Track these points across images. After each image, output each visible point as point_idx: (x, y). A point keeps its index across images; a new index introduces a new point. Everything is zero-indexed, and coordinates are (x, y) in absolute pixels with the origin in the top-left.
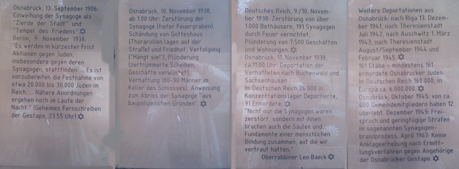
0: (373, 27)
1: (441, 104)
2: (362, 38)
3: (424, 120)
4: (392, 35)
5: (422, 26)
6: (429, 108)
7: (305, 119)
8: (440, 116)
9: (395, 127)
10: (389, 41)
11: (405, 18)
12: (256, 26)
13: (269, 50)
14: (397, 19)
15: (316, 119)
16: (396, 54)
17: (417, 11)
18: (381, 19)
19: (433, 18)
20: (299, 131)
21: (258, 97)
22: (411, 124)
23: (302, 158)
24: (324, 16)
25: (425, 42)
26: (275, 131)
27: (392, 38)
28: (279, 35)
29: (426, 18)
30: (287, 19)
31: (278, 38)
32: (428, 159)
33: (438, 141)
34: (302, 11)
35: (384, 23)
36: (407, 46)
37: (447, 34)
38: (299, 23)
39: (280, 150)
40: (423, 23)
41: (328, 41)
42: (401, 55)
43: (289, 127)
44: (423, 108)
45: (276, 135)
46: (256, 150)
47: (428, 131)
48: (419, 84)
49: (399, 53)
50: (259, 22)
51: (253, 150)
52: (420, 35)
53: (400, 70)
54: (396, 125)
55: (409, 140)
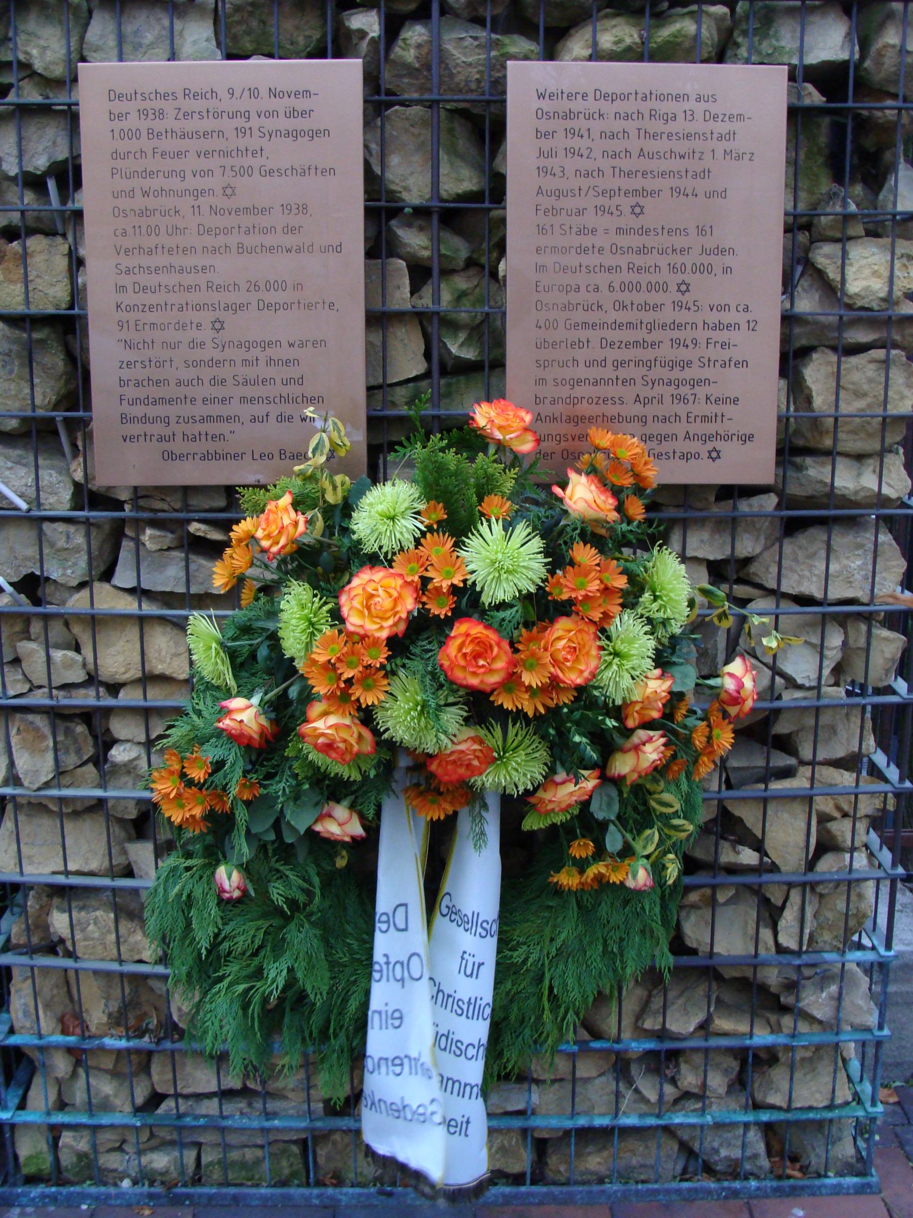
0: (569, 136)
1: (729, 326)
2: (543, 162)
3: (689, 364)
4: (615, 156)
5: (688, 136)
6: (702, 335)
7: (262, 363)
8: (725, 355)
9: (621, 378)
10: (608, 172)
11: (647, 116)
12: (134, 134)
13: (169, 193)
14: (627, 117)
15: (287, 362)
16: (626, 203)
17: (677, 98)
18: (589, 117)
19: (715, 117)
20: (249, 391)
21: (147, 309)
22: (658, 372)
23: (257, 456)
24: (301, 104)
25: (695, 176)
26: (190, 392)
27: (616, 162)
28: (192, 156)
29: (699, 115)
30: (211, 115)
31: (191, 163)
32: (697, 456)
33: (719, 414)
34: (247, 93)
35: (597, 126)
36: (651, 184)
37: (747, 157)
38: (240, 122)
39: (203, 437)
40: (691, 128)
41: (313, 167)
42: (638, 205)
43: (223, 382)
44: (686, 335)
45: (193, 400)
46: (148, 438)
47: (697, 389)
48: (680, 277)
49: (632, 201)
50: (144, 125)
51: (142, 439)
52: (682, 157)
53: (636, 241)
54: (623, 373)
55: (650, 411)
